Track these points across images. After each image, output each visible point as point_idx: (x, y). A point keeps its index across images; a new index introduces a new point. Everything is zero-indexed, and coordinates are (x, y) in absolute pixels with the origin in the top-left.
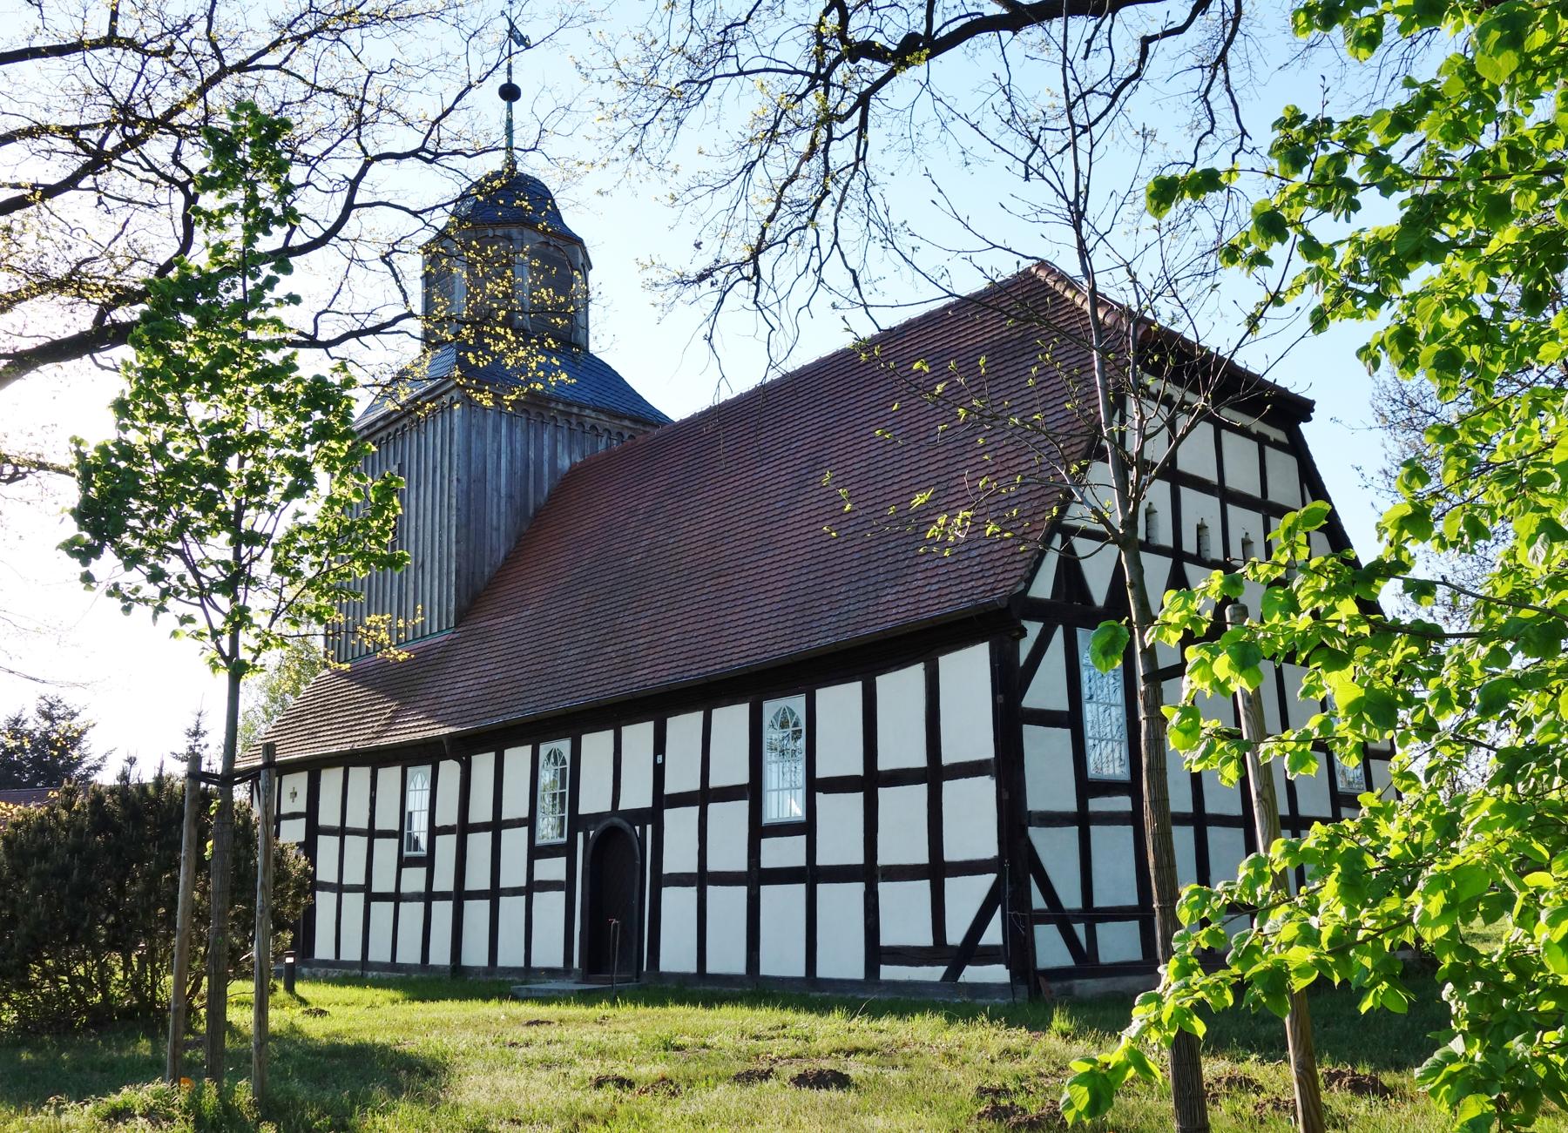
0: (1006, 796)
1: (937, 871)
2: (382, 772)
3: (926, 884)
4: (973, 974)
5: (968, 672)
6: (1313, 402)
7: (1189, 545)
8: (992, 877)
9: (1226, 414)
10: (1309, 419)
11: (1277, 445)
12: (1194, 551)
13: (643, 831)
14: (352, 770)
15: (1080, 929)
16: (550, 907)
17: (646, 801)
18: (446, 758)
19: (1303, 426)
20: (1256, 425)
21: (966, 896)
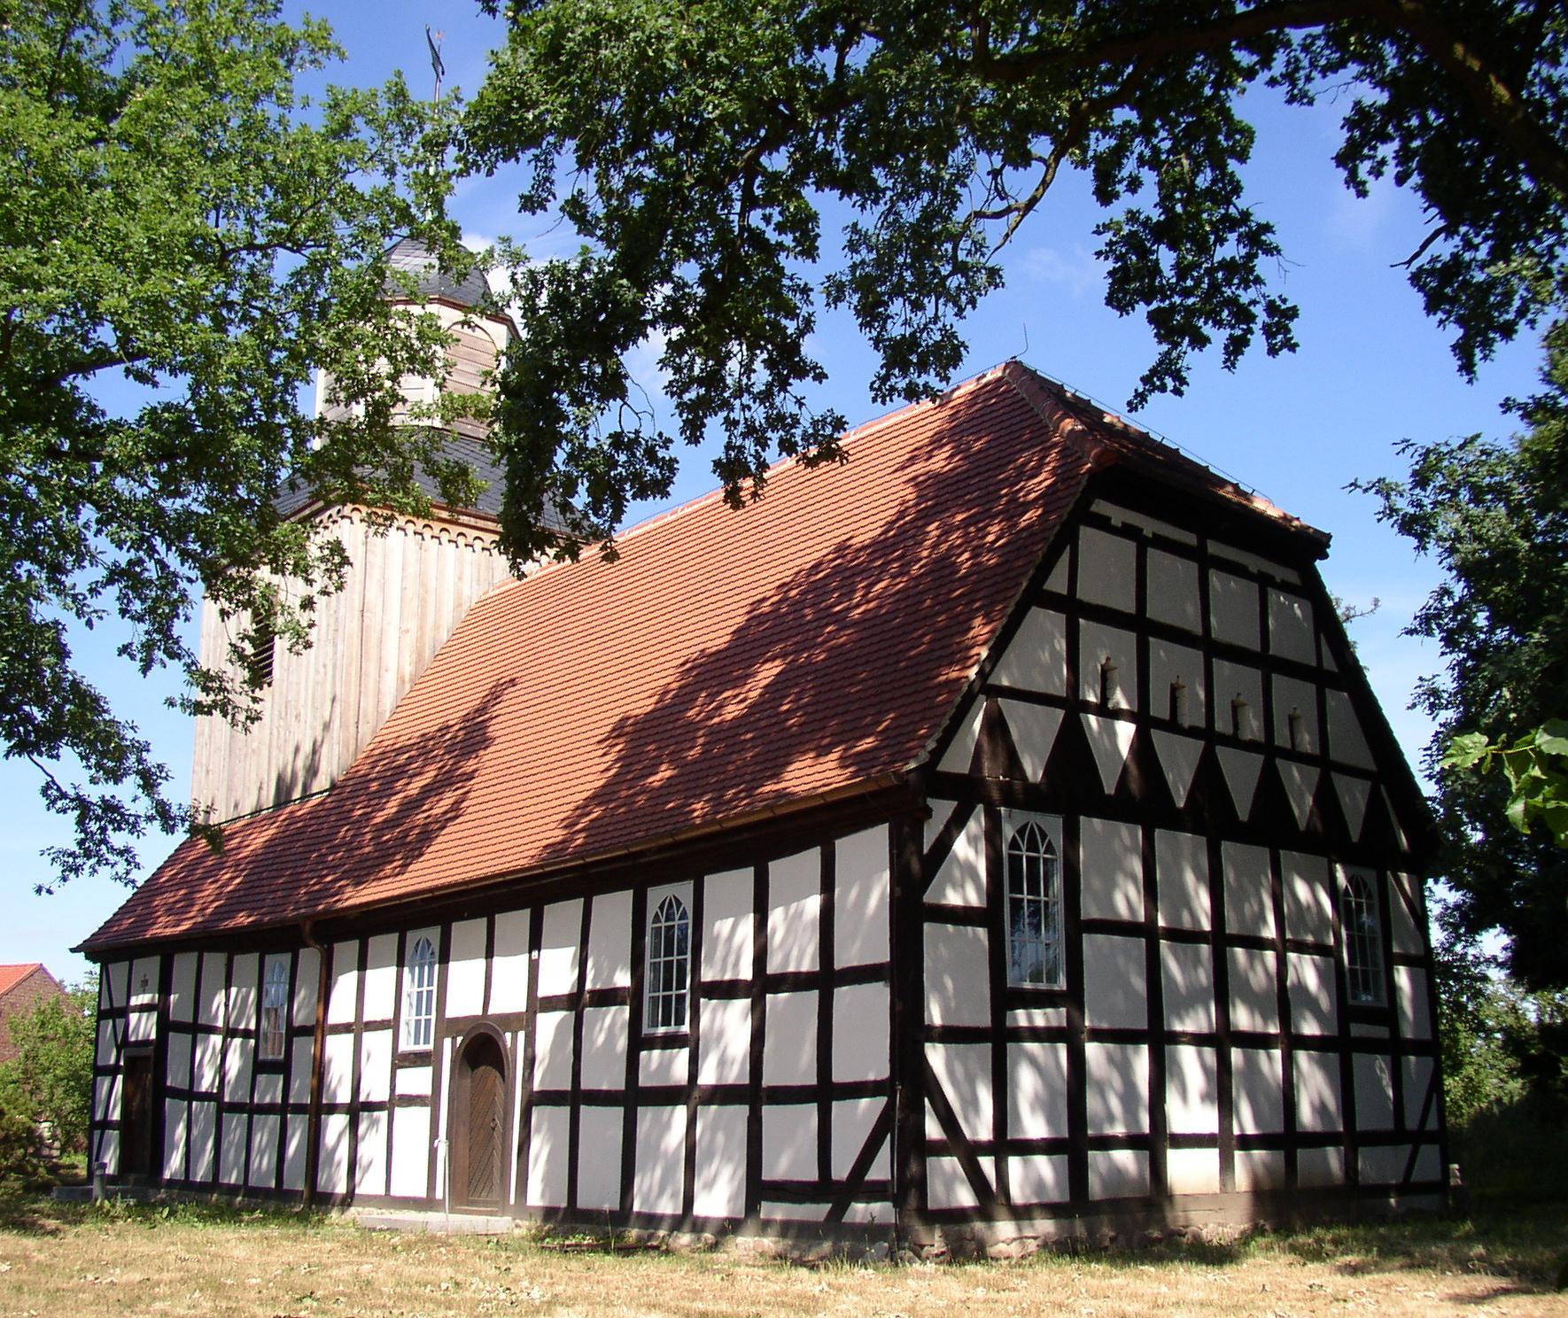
0: (899, 1007)
1: (825, 1092)
2: (238, 959)
3: (620, 1111)
4: (860, 1211)
5: (866, 863)
6: (1329, 537)
7: (1159, 708)
8: (882, 1101)
9: (1213, 548)
10: (1325, 556)
11: (1285, 587)
12: (1166, 715)
13: (514, 1039)
14: (206, 956)
15: (987, 1164)
16: (414, 1122)
17: (519, 1005)
18: (306, 946)
19: (1319, 564)
20: (1254, 563)
21: (857, 1119)
